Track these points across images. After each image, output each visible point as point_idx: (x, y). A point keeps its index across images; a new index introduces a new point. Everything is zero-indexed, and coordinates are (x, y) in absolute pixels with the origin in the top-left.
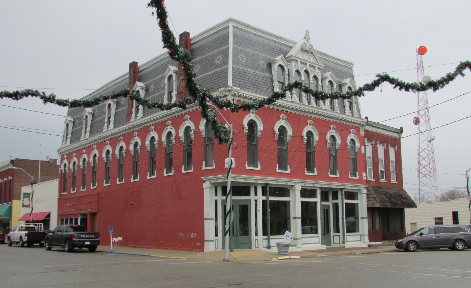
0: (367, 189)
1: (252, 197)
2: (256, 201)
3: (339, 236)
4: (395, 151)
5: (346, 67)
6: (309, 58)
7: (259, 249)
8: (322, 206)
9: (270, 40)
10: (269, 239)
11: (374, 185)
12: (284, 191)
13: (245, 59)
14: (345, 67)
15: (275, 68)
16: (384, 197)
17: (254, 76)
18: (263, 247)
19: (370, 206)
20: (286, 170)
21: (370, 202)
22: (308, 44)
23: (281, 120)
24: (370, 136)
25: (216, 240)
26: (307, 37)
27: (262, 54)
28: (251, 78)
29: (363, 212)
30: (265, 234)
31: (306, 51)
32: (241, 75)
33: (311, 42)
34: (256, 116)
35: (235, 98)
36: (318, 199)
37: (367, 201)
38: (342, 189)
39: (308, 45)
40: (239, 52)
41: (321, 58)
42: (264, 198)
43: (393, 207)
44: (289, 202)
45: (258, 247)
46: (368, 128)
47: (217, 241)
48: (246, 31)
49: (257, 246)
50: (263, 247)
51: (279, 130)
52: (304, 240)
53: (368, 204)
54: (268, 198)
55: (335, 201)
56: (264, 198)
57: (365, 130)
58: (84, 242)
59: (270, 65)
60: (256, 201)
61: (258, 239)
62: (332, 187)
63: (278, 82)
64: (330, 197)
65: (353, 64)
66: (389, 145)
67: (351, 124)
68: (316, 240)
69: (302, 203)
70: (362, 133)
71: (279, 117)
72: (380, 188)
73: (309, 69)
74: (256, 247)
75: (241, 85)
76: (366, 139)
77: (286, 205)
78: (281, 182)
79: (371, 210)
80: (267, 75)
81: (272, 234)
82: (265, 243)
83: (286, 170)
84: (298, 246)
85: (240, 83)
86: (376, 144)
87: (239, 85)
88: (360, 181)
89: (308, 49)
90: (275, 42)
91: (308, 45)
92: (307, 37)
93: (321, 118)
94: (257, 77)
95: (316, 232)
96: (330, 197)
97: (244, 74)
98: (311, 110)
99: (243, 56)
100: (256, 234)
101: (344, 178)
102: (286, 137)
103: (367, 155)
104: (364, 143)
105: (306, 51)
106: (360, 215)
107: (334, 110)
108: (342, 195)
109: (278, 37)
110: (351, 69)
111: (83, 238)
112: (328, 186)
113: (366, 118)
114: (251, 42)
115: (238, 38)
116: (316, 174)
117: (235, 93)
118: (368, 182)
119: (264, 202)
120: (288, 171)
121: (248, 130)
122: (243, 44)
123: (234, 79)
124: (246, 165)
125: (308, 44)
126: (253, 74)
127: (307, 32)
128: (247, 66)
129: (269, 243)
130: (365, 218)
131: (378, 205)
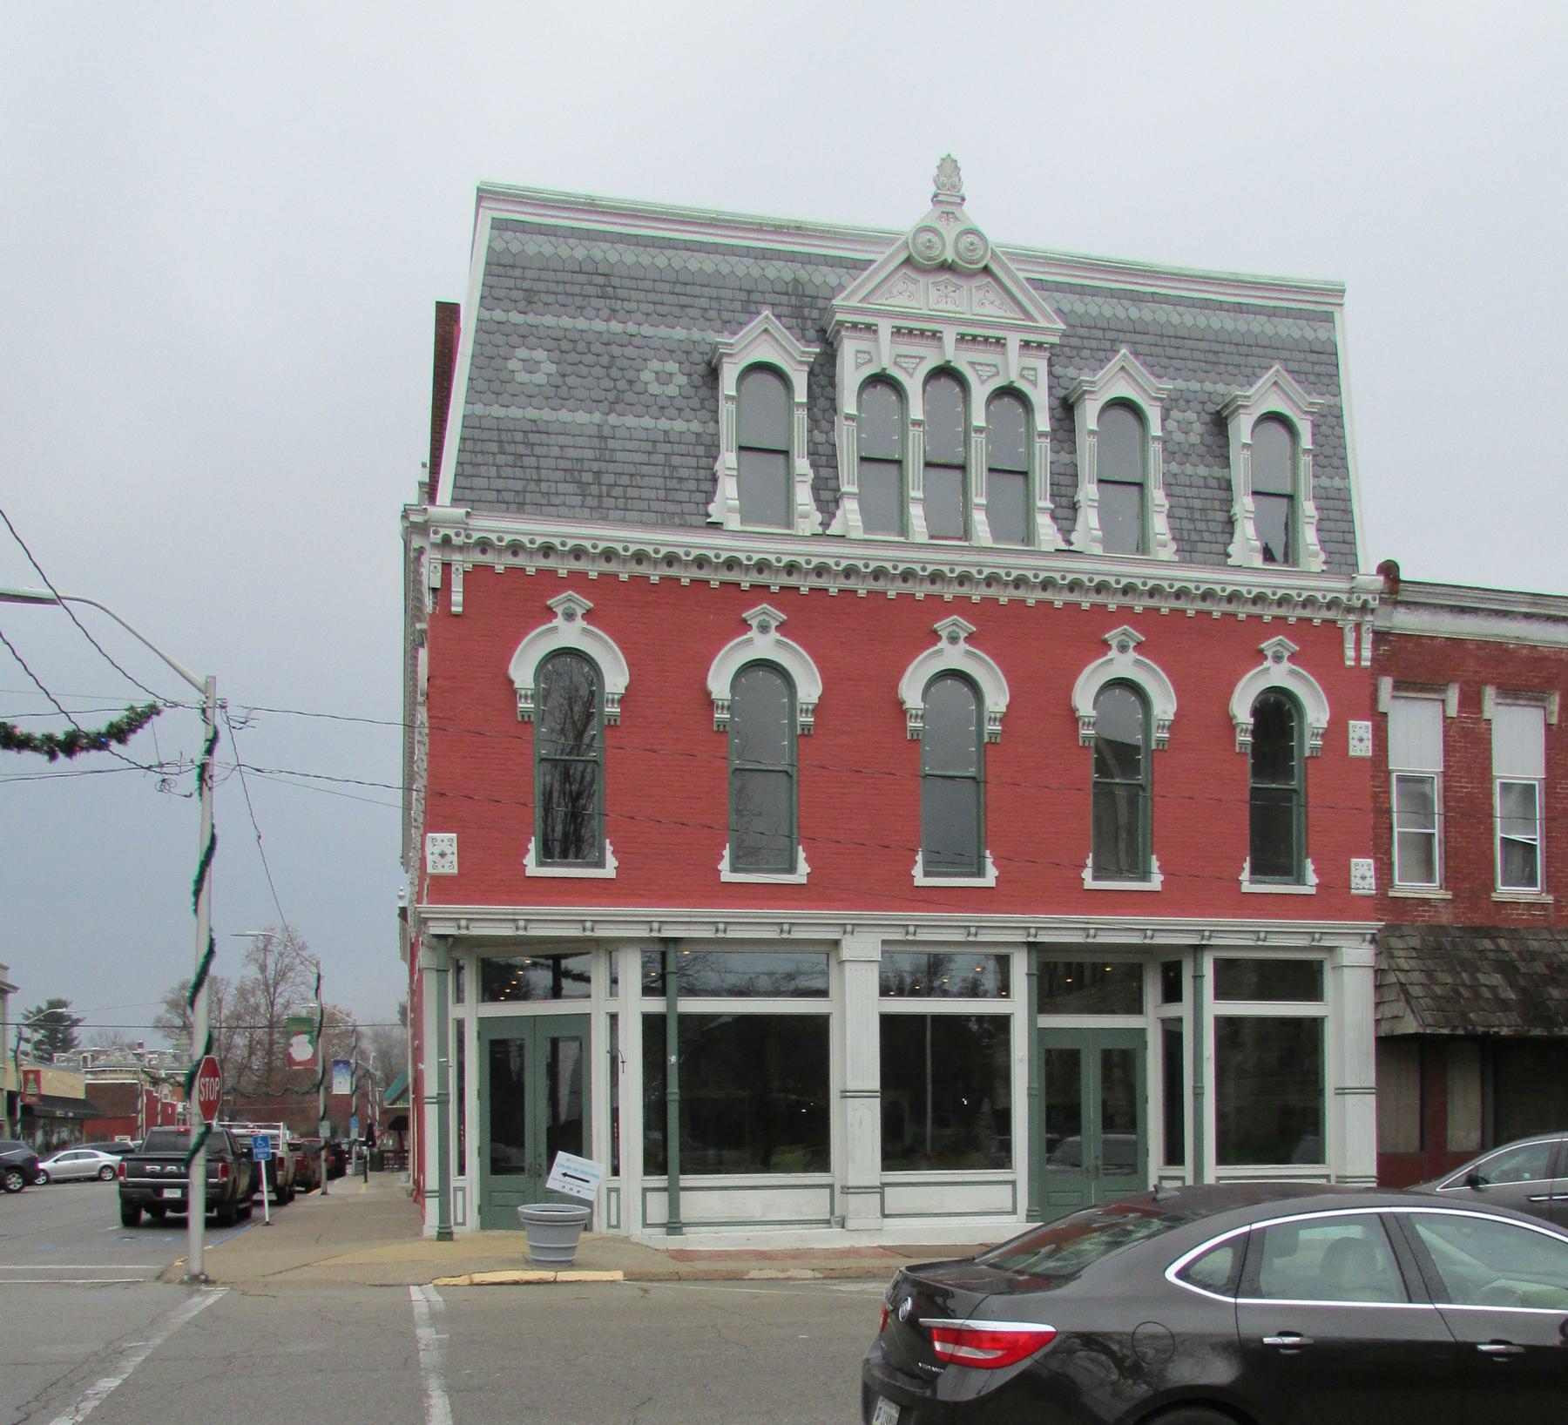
0: (1373, 941)
1: (597, 1006)
2: (614, 1018)
3: (1013, 1183)
4: (1548, 726)
5: (1288, 313)
6: (976, 304)
7: (622, 1232)
8: (1039, 1036)
9: (732, 251)
10: (673, 1191)
11: (1445, 918)
12: (1302, 977)
13: (552, 368)
14: (1273, 313)
15: (1242, 429)
16: (1496, 979)
17: (596, 443)
18: (645, 1225)
19: (1385, 1029)
20: (1300, 880)
21: (1388, 1011)
22: (950, 232)
23: (559, 622)
24: (1416, 665)
25: (610, 1190)
26: (948, 196)
27: (663, 331)
28: (571, 453)
29: (1349, 1059)
30: (655, 1162)
31: (946, 267)
32: (510, 448)
33: (975, 212)
34: (1292, 672)
35: (457, 557)
36: (1017, 1006)
37: (1377, 1005)
38: (1197, 950)
39: (950, 239)
40: (515, 340)
41: (1039, 284)
42: (656, 1005)
43: (1537, 1032)
44: (1316, 1024)
45: (618, 1226)
46: (1406, 621)
47: (460, 1194)
48: (574, 233)
49: (614, 1222)
50: (645, 1225)
51: (1260, 711)
52: (897, 1199)
53: (1377, 1021)
54: (671, 1005)
55: (1172, 1010)
56: (656, 1005)
57: (1380, 636)
58: (158, 1189)
59: (1220, 423)
60: (614, 1018)
61: (617, 1190)
62: (1160, 940)
63: (1255, 493)
64: (1152, 991)
65: (1343, 291)
66: (1489, 693)
67: (1268, 614)
68: (1001, 1196)
69: (889, 1023)
70: (1358, 652)
71: (935, 632)
72: (1490, 933)
73: (961, 360)
74: (610, 1226)
75: (508, 496)
76: (1386, 684)
77: (1310, 1030)
78: (1285, 937)
79: (1389, 1047)
80: (1202, 470)
81: (695, 1164)
82: (658, 1207)
83: (1300, 880)
84: (850, 1224)
85: (500, 484)
86: (1471, 701)
87: (492, 496)
88: (1334, 899)
89: (950, 256)
90: (764, 255)
91: (950, 239)
92: (948, 196)
93: (1032, 597)
94: (612, 444)
95: (1003, 1159)
96: (1152, 991)
97: (533, 438)
98: (953, 564)
99: (540, 354)
100: (462, 1170)
101: (1198, 889)
102: (1301, 736)
103: (1399, 763)
104: (1374, 700)
105: (946, 267)
106: (1332, 1077)
107: (1295, 564)
108: (1198, 978)
109: (779, 229)
110: (1328, 318)
111: (153, 1175)
112: (507, 931)
113: (1389, 569)
114: (600, 280)
115: (517, 273)
116: (1156, 882)
117: (1366, 601)
118: (1385, 904)
119: (653, 1026)
120: (610, 870)
121: (1254, 733)
122: (551, 299)
123: (468, 470)
124: (1245, 876)
125: (950, 232)
126: (594, 431)
127: (949, 168)
128: (558, 394)
129: (674, 1206)
130: (1361, 1091)
131: (1410, 1026)
